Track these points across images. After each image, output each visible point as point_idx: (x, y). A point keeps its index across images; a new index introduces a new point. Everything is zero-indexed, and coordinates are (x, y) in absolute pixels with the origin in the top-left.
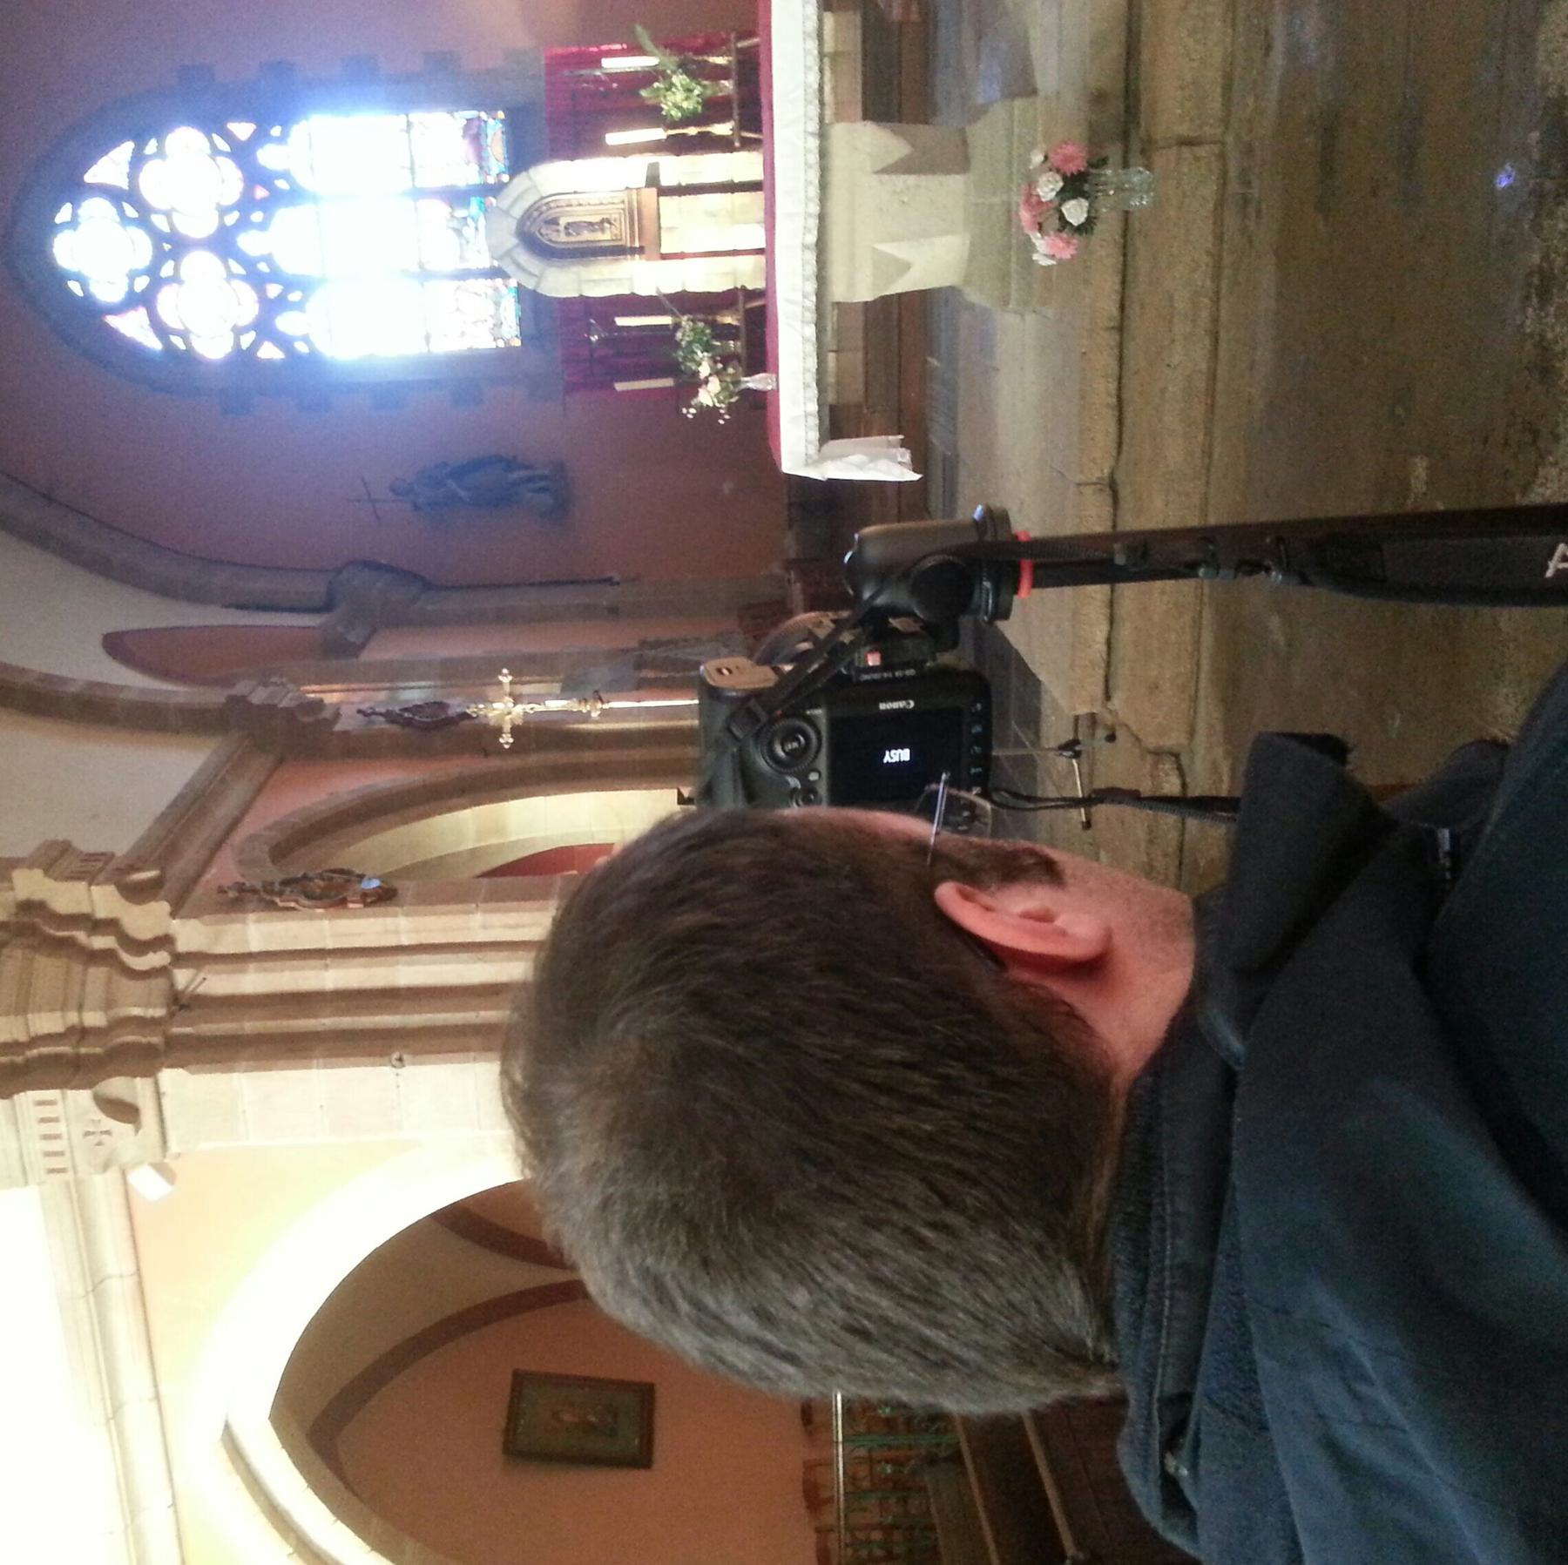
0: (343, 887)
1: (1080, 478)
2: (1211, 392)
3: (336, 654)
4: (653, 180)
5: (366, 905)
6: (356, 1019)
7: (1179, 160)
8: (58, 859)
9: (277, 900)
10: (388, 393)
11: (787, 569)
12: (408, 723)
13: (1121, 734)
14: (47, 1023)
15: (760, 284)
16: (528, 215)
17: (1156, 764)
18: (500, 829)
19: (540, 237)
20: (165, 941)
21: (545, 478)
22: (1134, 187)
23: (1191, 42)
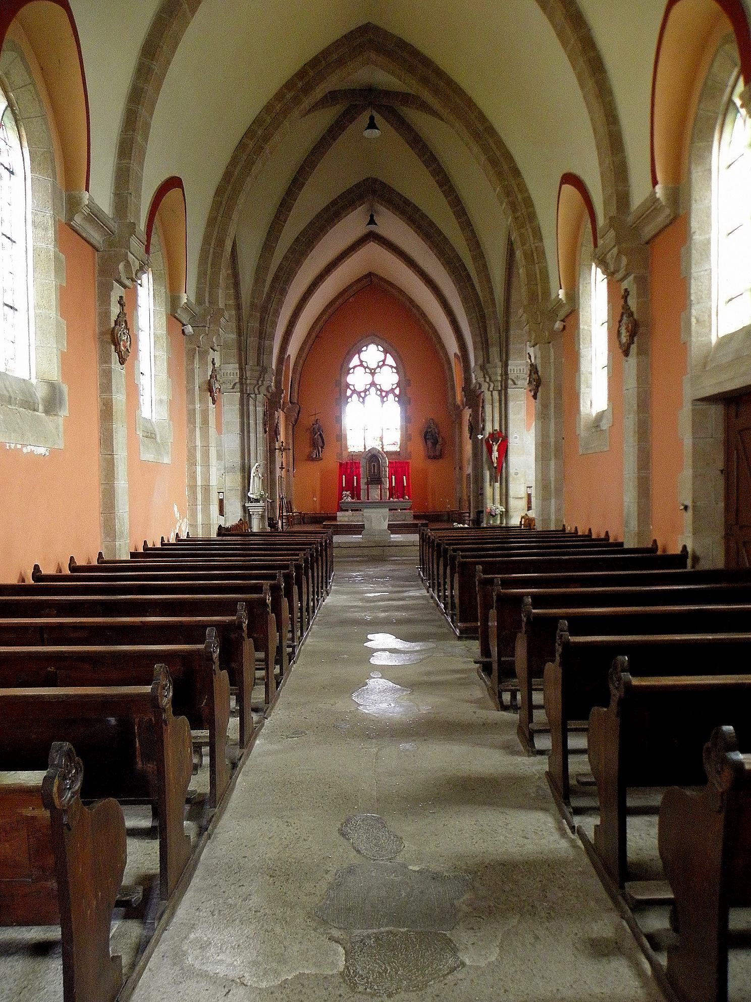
10: (339, 419)
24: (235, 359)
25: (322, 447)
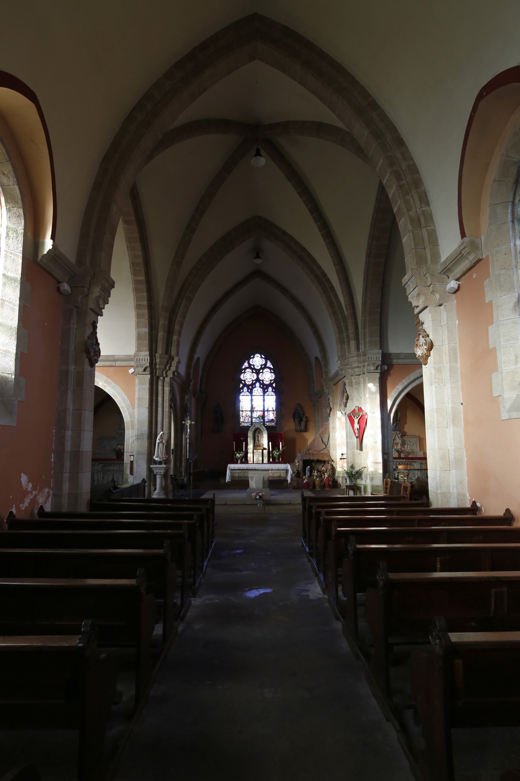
4: (265, 449)
14: (158, 360)
19: (257, 432)
20: (167, 376)
22: (260, 504)
24: (146, 348)
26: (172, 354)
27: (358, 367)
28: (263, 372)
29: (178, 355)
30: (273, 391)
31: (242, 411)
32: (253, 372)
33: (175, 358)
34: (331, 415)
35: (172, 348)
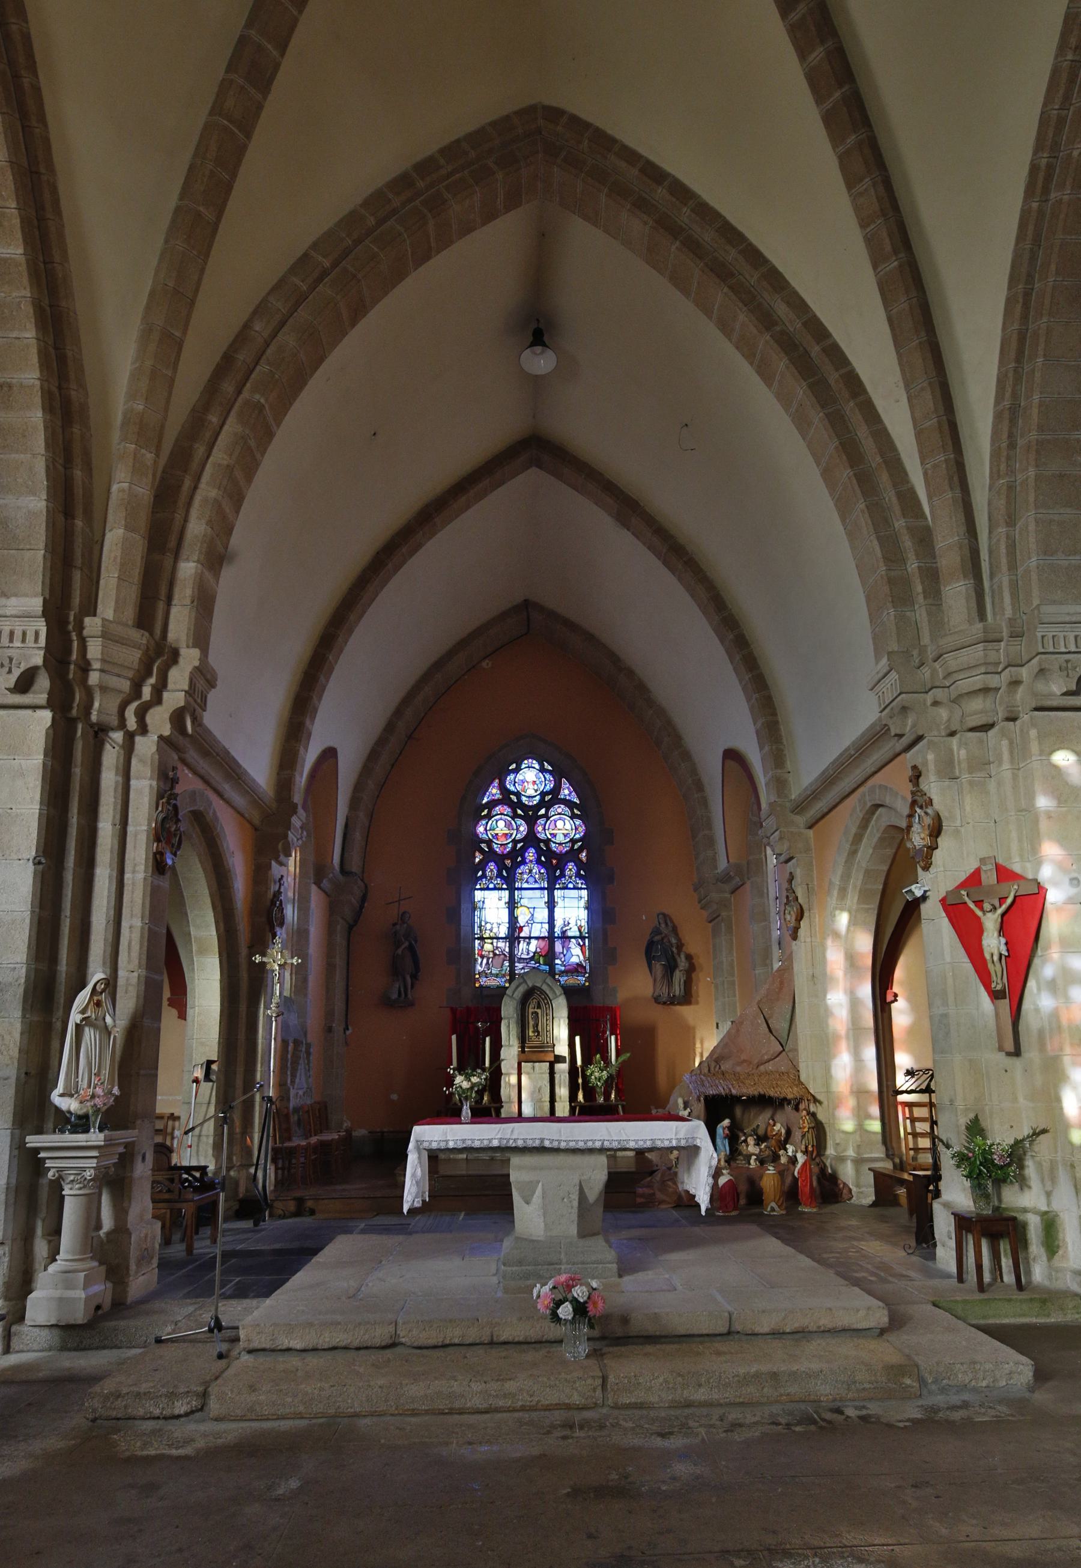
0: (168, 842)
1: (400, 1321)
2: (451, 1412)
3: (315, 871)
4: (559, 1059)
5: (155, 854)
6: (74, 838)
7: (593, 1377)
8: (204, 678)
9: (164, 800)
11: (346, 1131)
12: (273, 903)
13: (224, 1362)
15: (503, 1115)
16: (543, 992)
17: (197, 1395)
18: (202, 951)
19: (532, 1000)
21: (406, 995)
23: (661, 1379)
25: (414, 977)
26: (171, 636)
27: (986, 690)
28: (546, 816)
29: (201, 639)
30: (578, 875)
31: (482, 939)
32: (515, 816)
33: (183, 651)
34: (802, 933)
35: (174, 611)
